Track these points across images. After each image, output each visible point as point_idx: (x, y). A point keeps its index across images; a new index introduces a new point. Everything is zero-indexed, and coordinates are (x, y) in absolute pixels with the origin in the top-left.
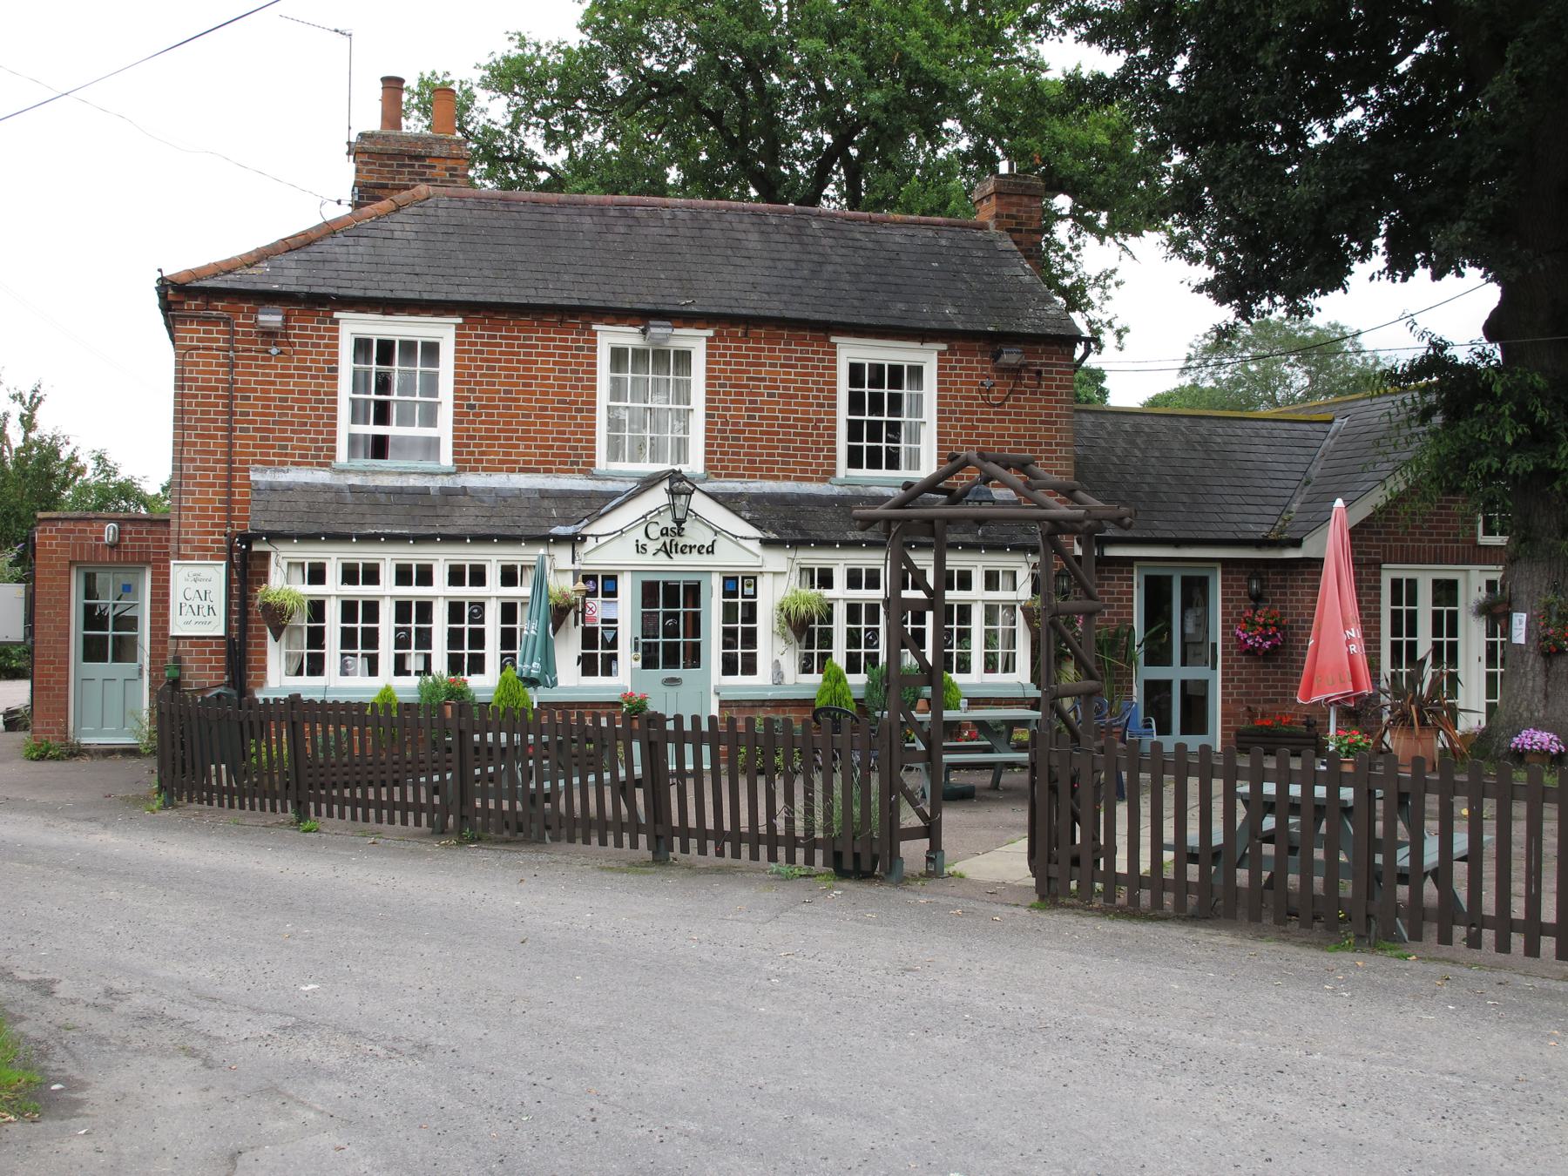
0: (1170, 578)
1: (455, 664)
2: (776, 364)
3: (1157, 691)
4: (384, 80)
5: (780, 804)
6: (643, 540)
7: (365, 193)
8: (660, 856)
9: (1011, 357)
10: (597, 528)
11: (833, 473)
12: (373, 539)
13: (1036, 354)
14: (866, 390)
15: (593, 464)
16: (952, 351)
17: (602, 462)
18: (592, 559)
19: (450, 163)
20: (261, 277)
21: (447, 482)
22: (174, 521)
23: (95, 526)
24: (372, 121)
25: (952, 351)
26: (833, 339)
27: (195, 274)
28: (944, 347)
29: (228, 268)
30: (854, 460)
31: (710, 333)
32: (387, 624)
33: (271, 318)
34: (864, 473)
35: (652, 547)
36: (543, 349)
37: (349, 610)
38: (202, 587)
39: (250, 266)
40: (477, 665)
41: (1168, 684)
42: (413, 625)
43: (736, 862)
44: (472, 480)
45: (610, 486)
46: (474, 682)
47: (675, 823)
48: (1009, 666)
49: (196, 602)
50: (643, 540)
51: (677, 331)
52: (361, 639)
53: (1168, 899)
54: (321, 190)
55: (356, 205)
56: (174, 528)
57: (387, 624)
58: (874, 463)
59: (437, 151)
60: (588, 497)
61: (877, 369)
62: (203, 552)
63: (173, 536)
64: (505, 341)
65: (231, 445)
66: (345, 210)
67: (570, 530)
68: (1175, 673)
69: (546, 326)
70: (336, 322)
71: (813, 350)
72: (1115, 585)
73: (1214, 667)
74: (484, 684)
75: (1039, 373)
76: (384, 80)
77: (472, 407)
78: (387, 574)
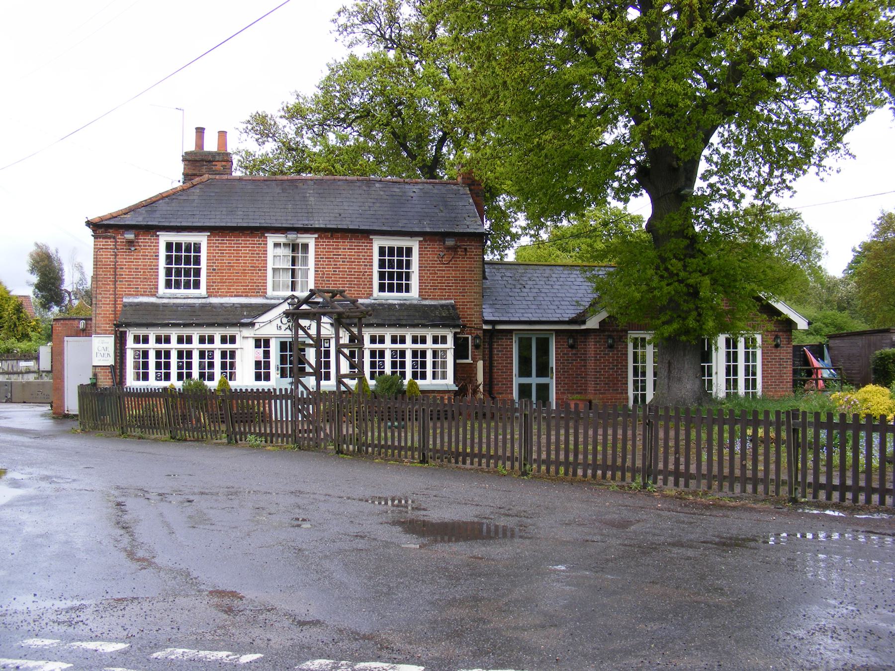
0: (531, 339)
1: (202, 375)
2: (345, 249)
3: (524, 390)
4: (197, 129)
5: (476, 436)
6: (280, 324)
7: (187, 176)
8: (424, 461)
9: (450, 242)
10: (261, 319)
11: (371, 295)
12: (166, 325)
13: (463, 241)
14: (387, 258)
15: (266, 293)
16: (425, 240)
17: (270, 292)
18: (257, 332)
19: (224, 163)
20: (129, 220)
21: (203, 301)
22: (94, 319)
23: (76, 321)
24: (191, 147)
25: (425, 240)
26: (371, 237)
27: (102, 219)
28: (421, 239)
29: (113, 217)
30: (382, 288)
31: (316, 236)
32: (174, 360)
33: (130, 236)
34: (387, 294)
35: (284, 327)
36: (245, 244)
37: (158, 354)
38: (105, 346)
39: (125, 214)
40: (211, 378)
41: (530, 385)
42: (185, 360)
43: (463, 466)
44: (214, 300)
45: (273, 302)
46: (207, 383)
47: (431, 447)
48: (444, 377)
49: (102, 352)
50: (280, 324)
51: (299, 235)
52: (163, 366)
53: (875, 498)
54: (170, 176)
55: (184, 183)
56: (94, 322)
57: (174, 360)
58: (391, 289)
59: (217, 158)
60: (263, 305)
61: (391, 249)
62: (105, 332)
63: (93, 325)
64: (229, 243)
65: (115, 288)
66: (181, 184)
67: (249, 320)
68: (534, 380)
69: (246, 236)
70: (158, 236)
71: (363, 243)
72: (504, 342)
73: (552, 378)
74: (213, 385)
75: (466, 249)
76: (197, 129)
77: (214, 270)
78: (217, 339)
